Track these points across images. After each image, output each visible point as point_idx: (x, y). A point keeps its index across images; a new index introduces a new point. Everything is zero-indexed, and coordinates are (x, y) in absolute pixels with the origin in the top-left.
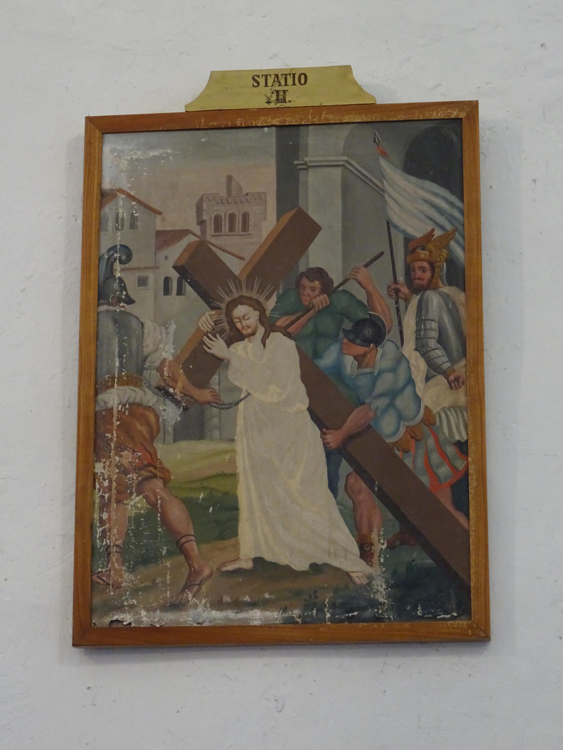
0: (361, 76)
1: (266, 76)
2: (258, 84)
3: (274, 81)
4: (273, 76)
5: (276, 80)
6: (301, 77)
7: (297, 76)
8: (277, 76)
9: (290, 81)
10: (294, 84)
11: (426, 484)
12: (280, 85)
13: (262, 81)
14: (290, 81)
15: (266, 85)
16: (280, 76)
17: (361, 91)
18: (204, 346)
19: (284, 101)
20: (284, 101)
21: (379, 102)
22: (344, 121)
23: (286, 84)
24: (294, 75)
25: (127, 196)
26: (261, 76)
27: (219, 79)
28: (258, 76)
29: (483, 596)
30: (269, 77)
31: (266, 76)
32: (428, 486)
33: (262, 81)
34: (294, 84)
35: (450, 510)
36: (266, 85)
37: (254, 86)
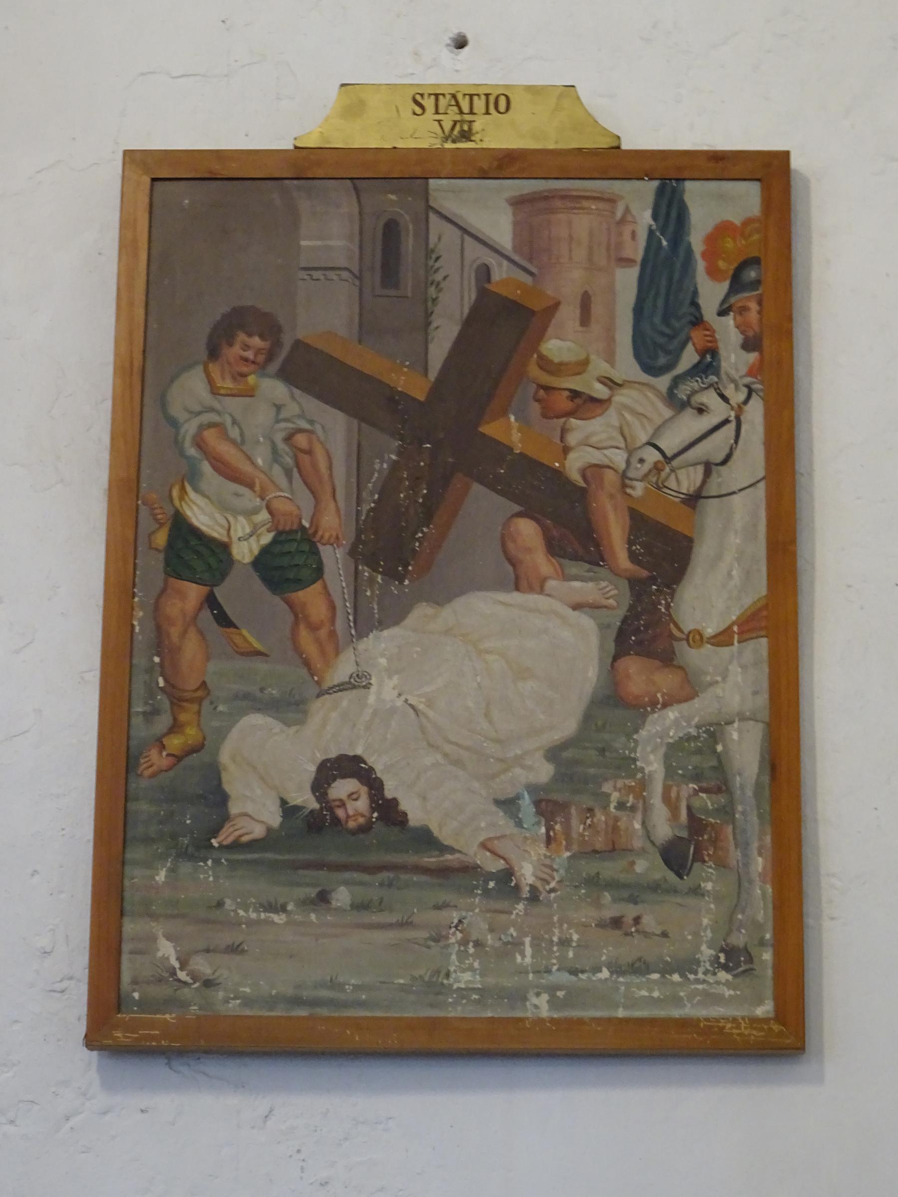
1: (471, 96)
4: (448, 97)
5: (453, 103)
6: (498, 102)
7: (492, 99)
8: (454, 96)
9: (479, 105)
11: (294, 594)
12: (461, 112)
13: (429, 103)
14: (479, 105)
16: (460, 97)
18: (672, 625)
19: (466, 135)
20: (466, 135)
23: (471, 112)
26: (426, 96)
28: (422, 95)
30: (441, 97)
32: (290, 594)
33: (429, 103)
34: (487, 113)
35: (760, 429)
37: (415, 114)
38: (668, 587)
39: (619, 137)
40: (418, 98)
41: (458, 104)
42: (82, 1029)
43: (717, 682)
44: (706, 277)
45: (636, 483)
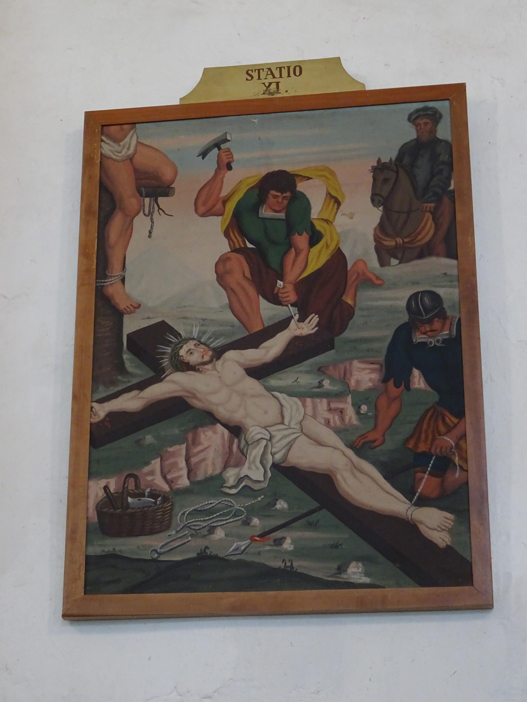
0: (351, 67)
1: (280, 68)
2: (252, 77)
3: (267, 74)
4: (266, 70)
5: (269, 73)
6: (296, 69)
8: (270, 69)
9: (285, 73)
10: (289, 76)
12: (274, 77)
13: (255, 75)
14: (285, 73)
15: (259, 78)
17: (353, 81)
21: (371, 86)
22: (128, 125)
24: (289, 68)
25: (105, 277)
27: (211, 75)
28: (252, 71)
29: (207, 518)
30: (261, 71)
31: (259, 70)
33: (255, 75)
34: (289, 76)
36: (259, 78)
37: (247, 80)
38: (202, 552)
39: (364, 85)
40: (250, 72)
41: (272, 73)
42: (182, 97)
43: (258, 536)
44: (444, 114)
45: (398, 241)
